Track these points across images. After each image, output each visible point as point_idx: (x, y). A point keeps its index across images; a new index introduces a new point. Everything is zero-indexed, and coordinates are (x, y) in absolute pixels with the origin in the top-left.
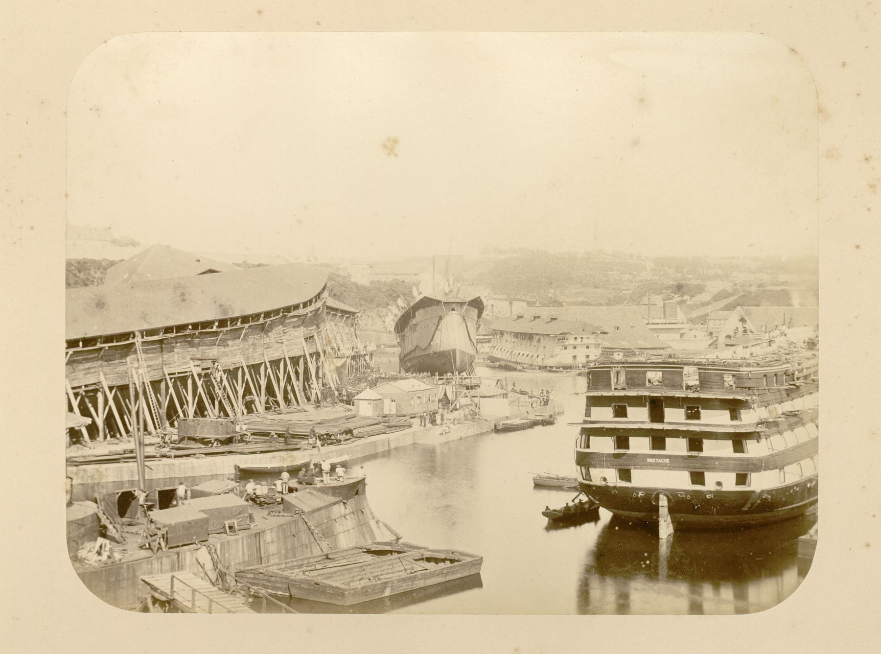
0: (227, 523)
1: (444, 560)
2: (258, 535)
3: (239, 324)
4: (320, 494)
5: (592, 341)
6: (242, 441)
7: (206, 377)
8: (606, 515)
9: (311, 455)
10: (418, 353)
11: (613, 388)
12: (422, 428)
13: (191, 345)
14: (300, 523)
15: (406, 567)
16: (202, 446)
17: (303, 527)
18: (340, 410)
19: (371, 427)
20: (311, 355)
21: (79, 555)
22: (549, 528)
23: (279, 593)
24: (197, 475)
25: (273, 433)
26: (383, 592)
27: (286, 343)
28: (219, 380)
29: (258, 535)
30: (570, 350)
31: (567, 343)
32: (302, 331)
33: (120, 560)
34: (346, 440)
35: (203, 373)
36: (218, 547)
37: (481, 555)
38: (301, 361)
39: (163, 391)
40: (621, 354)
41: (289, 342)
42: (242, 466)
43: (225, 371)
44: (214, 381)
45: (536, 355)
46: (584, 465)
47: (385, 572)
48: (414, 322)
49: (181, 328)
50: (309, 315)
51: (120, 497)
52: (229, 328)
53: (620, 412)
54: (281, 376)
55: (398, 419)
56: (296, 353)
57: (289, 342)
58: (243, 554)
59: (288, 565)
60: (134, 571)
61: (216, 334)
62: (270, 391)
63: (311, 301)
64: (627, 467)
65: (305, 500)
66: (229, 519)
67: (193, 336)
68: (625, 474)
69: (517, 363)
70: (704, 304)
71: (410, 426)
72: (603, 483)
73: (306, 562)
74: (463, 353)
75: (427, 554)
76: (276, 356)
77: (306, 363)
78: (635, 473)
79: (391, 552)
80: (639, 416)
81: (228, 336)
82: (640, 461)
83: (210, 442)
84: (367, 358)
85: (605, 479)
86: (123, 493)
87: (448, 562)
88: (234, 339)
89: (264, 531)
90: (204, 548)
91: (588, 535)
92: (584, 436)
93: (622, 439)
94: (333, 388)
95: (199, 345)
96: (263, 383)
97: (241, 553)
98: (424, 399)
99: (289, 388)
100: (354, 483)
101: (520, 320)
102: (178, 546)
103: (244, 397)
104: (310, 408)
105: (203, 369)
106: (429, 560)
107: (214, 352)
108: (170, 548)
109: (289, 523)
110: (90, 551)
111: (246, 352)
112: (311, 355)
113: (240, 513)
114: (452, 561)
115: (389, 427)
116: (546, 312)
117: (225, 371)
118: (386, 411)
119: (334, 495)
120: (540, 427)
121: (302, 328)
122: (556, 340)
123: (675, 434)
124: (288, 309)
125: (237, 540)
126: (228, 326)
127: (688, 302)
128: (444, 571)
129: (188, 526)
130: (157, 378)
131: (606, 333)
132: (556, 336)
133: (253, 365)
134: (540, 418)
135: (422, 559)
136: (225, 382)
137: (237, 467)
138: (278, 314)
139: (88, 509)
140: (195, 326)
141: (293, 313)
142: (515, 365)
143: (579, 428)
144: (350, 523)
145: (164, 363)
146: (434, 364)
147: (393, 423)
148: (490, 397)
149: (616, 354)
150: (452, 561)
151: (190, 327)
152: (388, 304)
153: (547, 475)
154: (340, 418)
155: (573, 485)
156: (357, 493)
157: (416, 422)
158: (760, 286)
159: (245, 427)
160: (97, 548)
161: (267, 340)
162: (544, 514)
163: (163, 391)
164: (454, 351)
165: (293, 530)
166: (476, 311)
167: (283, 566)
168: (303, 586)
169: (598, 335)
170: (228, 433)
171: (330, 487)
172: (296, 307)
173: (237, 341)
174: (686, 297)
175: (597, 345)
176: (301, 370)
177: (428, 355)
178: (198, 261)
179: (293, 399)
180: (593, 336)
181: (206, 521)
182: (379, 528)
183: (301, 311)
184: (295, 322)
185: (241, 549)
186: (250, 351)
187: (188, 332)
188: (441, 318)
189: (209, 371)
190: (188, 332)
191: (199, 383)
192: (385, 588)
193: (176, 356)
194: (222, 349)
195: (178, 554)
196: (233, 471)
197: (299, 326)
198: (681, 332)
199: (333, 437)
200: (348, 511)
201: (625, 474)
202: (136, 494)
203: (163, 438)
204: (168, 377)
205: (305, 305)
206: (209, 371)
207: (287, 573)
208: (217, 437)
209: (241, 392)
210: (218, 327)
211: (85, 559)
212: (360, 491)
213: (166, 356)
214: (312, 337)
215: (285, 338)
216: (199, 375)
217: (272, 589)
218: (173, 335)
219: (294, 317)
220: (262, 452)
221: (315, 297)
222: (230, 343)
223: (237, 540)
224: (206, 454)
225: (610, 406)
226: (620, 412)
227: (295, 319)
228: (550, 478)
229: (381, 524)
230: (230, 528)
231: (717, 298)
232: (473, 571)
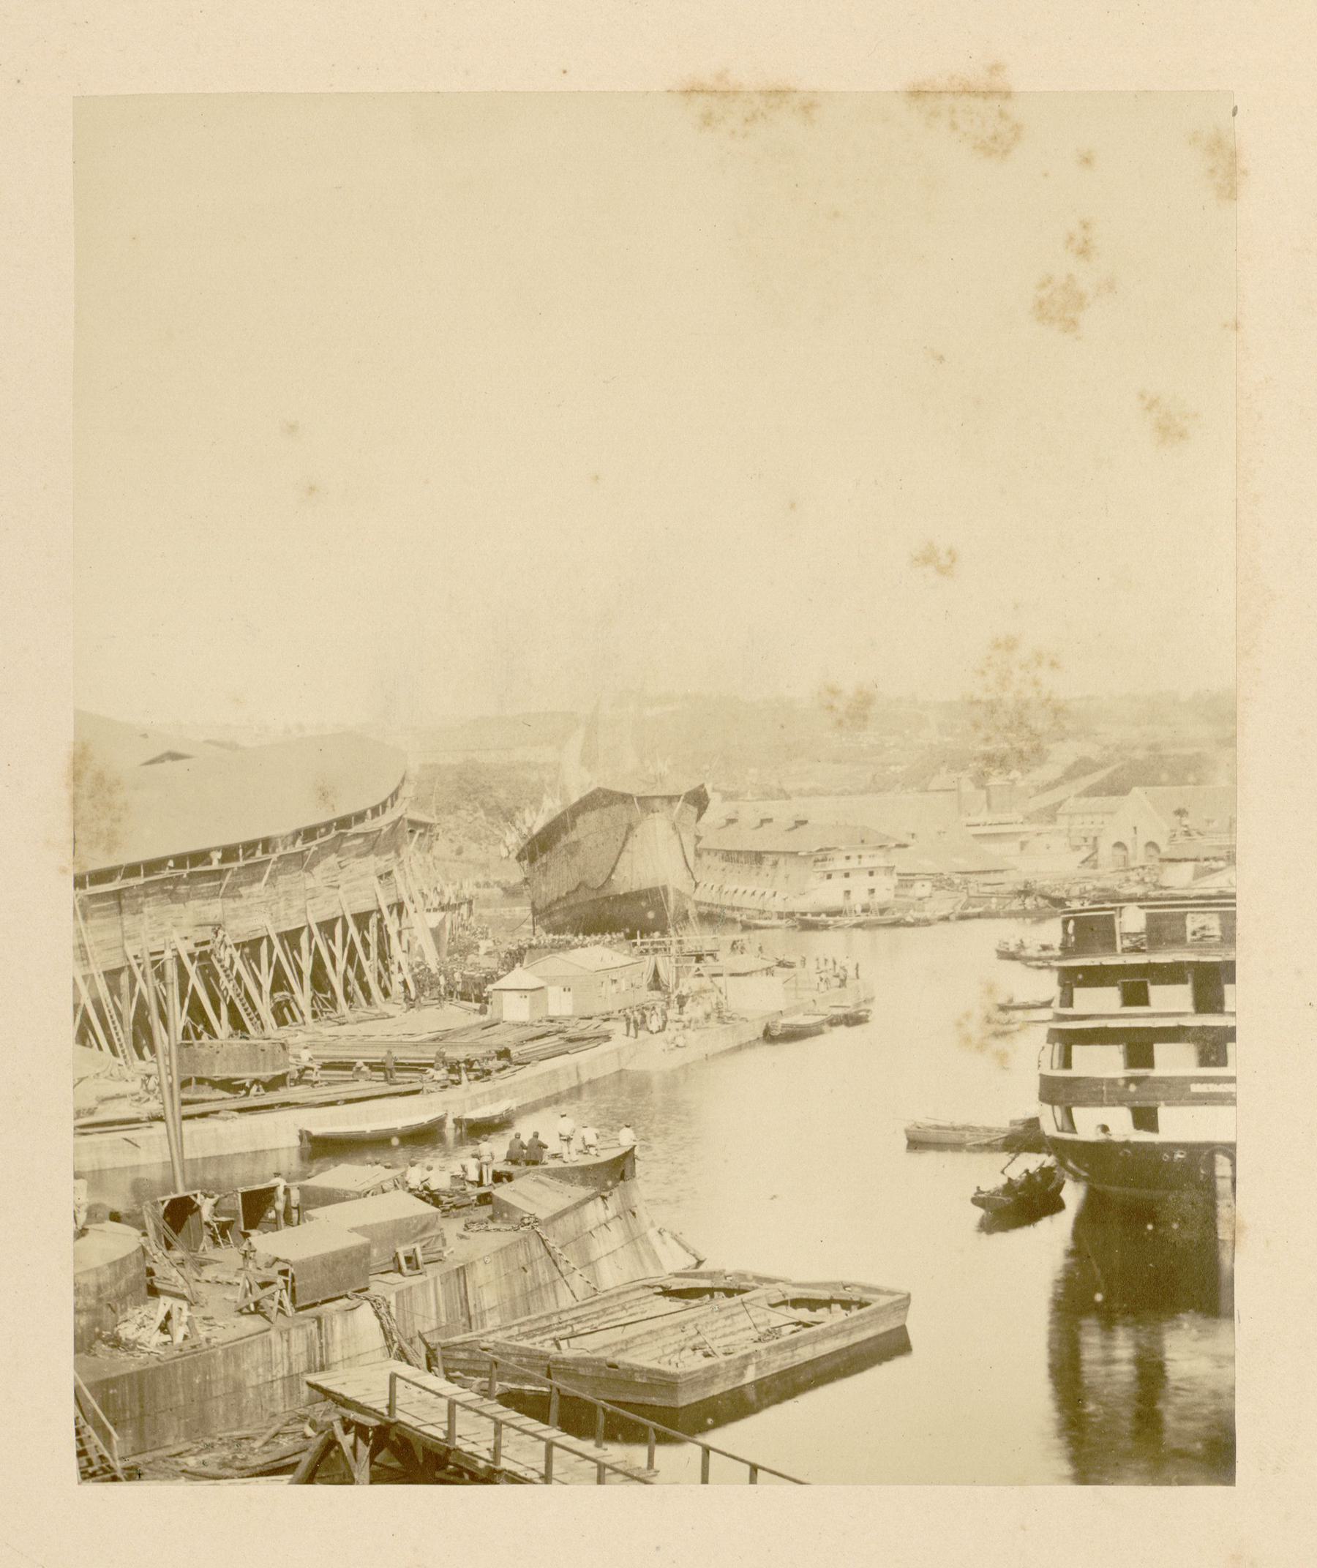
0: (402, 1251)
1: (827, 1303)
2: (461, 1271)
3: (259, 853)
4: (556, 1182)
5: (880, 861)
6: (299, 1081)
7: (204, 958)
8: (1073, 1194)
9: (445, 1103)
10: (583, 896)
11: (1119, 949)
12: (631, 1040)
13: (174, 897)
14: (534, 1242)
15: (756, 1320)
16: (225, 1094)
17: (538, 1251)
18: (457, 1015)
19: (537, 1043)
20: (390, 907)
21: (122, 1334)
22: (987, 1227)
23: (527, 1387)
24: (226, 1153)
25: (360, 1063)
26: (742, 1375)
27: (344, 887)
28: (227, 964)
29: (461, 1271)
30: (838, 880)
31: (830, 867)
32: (374, 863)
33: (208, 1340)
34: (499, 1070)
35: (198, 951)
36: (392, 1299)
37: (905, 1288)
38: (373, 921)
39: (125, 990)
40: (928, 884)
41: (347, 886)
42: (317, 1131)
43: (237, 946)
44: (218, 966)
45: (769, 893)
46: (1059, 1103)
47: (720, 1333)
48: (573, 836)
49: (153, 866)
50: (385, 830)
51: (166, 1210)
52: (242, 863)
53: (1135, 996)
54: (337, 950)
55: (584, 1024)
56: (364, 905)
57: (347, 886)
58: (438, 1313)
59: (524, 1329)
60: (237, 1358)
61: (219, 874)
62: (320, 981)
63: (384, 805)
64: (1152, 1104)
65: (531, 1195)
66: (407, 1241)
67: (177, 881)
68: (1145, 1119)
69: (733, 908)
70: (1050, 786)
71: (608, 1038)
72: (1101, 1137)
73: (555, 1320)
74: (679, 893)
75: (794, 1293)
76: (326, 914)
77: (381, 920)
78: (1166, 1114)
79: (711, 1291)
80: (1171, 1002)
81: (242, 878)
82: (1178, 1091)
83: (242, 1087)
84: (464, 909)
85: (1105, 1129)
86: (173, 1202)
87: (836, 1307)
88: (251, 883)
89: (473, 1263)
90: (367, 1305)
91: (1051, 1238)
92: (1057, 1046)
93: (1139, 1047)
94: (434, 971)
95: (188, 897)
96: (307, 964)
97: (433, 1309)
98: (623, 984)
99: (351, 974)
100: (619, 1157)
101: (801, 828)
102: (314, 1305)
103: (273, 990)
104: (394, 1008)
105: (196, 945)
106: (796, 1303)
107: (214, 909)
108: (298, 1310)
109: (515, 1245)
110: (142, 1326)
111: (274, 908)
112: (390, 907)
113: (425, 1229)
114: (846, 1305)
115: (570, 1040)
116: (783, 812)
117: (237, 946)
118: (553, 1011)
119: (584, 1183)
120: (842, 1028)
121: (372, 857)
122: (811, 863)
123: (1174, 1035)
124: (344, 822)
125: (425, 1284)
126: (245, 860)
127: (1021, 784)
128: (848, 1326)
129: (332, 1262)
130: (116, 963)
131: (905, 846)
132: (810, 855)
133: (286, 933)
134: (840, 1012)
135: (784, 1303)
136: (239, 965)
137: (305, 1136)
138: (328, 832)
139: (118, 1242)
140: (180, 861)
141: (357, 829)
142: (728, 913)
143: (1043, 1031)
144: (615, 1236)
145: (126, 936)
146: (619, 915)
147: (572, 1033)
148: (745, 974)
149: (918, 884)
150: (846, 1305)
151: (171, 863)
152: (457, 808)
153: (932, 1123)
154: (469, 1028)
155: (986, 1141)
156: (622, 1177)
157: (618, 1028)
158: (1153, 747)
159: (305, 1055)
160: (160, 1318)
161: (310, 883)
162: (975, 1201)
163: (125, 990)
164: (665, 889)
165: (522, 1257)
166: (695, 810)
167: (514, 1331)
168: (582, 1371)
169: (889, 850)
170: (275, 1068)
171: (577, 1168)
172: (360, 817)
173: (258, 888)
174: (1016, 774)
175: (890, 869)
176: (372, 937)
177: (607, 899)
178: (145, 736)
179: (360, 993)
180: (880, 853)
181: (365, 1251)
182: (664, 1243)
183: (369, 825)
184: (358, 847)
185: (433, 1302)
186: (282, 904)
187: (166, 873)
188: (630, 828)
189: (207, 948)
190: (166, 873)
191: (192, 969)
192: (745, 1367)
193: (147, 921)
194: (232, 904)
195: (319, 1319)
196: (297, 1142)
197: (366, 854)
198: (1023, 838)
199: (476, 1066)
200: (610, 1214)
201: (1145, 1119)
202: (198, 1201)
203: (143, 1081)
204: (134, 962)
205: (375, 811)
206: (207, 948)
207: (525, 1343)
208: (256, 1075)
209: (267, 982)
210: (222, 861)
211: (135, 1342)
212: (627, 1173)
213: (128, 920)
214: (389, 873)
215: (342, 877)
216: (191, 956)
217: (513, 1380)
218: (141, 880)
219: (357, 836)
220: (348, 1101)
221: (392, 796)
222: (243, 890)
223: (425, 1284)
224: (240, 1110)
225: (1114, 985)
226: (1135, 996)
227: (360, 841)
228: (938, 1127)
229: (667, 1235)
230: (408, 1259)
231: (1071, 774)
232: (893, 1324)
